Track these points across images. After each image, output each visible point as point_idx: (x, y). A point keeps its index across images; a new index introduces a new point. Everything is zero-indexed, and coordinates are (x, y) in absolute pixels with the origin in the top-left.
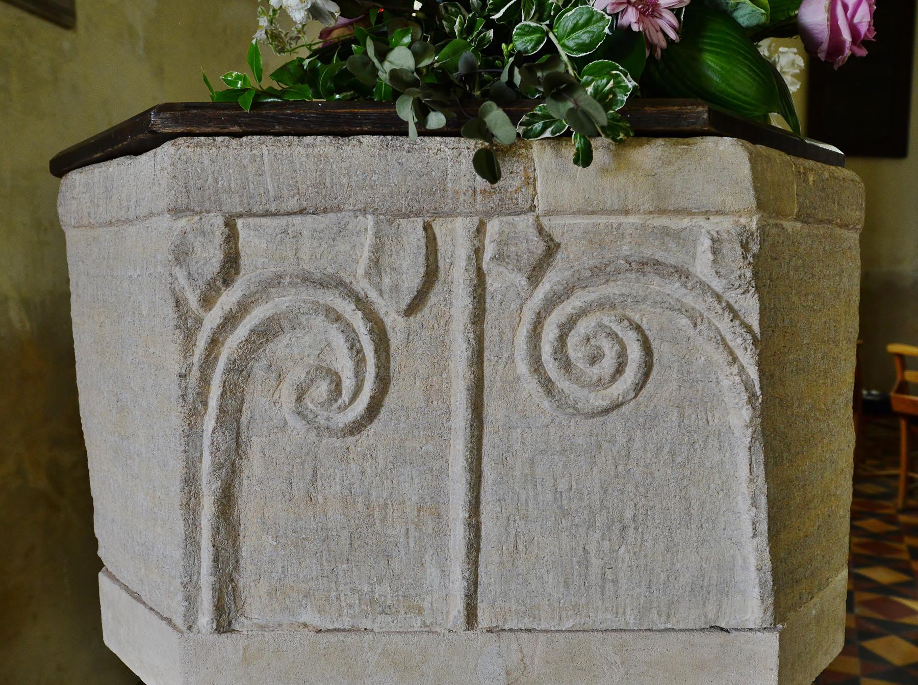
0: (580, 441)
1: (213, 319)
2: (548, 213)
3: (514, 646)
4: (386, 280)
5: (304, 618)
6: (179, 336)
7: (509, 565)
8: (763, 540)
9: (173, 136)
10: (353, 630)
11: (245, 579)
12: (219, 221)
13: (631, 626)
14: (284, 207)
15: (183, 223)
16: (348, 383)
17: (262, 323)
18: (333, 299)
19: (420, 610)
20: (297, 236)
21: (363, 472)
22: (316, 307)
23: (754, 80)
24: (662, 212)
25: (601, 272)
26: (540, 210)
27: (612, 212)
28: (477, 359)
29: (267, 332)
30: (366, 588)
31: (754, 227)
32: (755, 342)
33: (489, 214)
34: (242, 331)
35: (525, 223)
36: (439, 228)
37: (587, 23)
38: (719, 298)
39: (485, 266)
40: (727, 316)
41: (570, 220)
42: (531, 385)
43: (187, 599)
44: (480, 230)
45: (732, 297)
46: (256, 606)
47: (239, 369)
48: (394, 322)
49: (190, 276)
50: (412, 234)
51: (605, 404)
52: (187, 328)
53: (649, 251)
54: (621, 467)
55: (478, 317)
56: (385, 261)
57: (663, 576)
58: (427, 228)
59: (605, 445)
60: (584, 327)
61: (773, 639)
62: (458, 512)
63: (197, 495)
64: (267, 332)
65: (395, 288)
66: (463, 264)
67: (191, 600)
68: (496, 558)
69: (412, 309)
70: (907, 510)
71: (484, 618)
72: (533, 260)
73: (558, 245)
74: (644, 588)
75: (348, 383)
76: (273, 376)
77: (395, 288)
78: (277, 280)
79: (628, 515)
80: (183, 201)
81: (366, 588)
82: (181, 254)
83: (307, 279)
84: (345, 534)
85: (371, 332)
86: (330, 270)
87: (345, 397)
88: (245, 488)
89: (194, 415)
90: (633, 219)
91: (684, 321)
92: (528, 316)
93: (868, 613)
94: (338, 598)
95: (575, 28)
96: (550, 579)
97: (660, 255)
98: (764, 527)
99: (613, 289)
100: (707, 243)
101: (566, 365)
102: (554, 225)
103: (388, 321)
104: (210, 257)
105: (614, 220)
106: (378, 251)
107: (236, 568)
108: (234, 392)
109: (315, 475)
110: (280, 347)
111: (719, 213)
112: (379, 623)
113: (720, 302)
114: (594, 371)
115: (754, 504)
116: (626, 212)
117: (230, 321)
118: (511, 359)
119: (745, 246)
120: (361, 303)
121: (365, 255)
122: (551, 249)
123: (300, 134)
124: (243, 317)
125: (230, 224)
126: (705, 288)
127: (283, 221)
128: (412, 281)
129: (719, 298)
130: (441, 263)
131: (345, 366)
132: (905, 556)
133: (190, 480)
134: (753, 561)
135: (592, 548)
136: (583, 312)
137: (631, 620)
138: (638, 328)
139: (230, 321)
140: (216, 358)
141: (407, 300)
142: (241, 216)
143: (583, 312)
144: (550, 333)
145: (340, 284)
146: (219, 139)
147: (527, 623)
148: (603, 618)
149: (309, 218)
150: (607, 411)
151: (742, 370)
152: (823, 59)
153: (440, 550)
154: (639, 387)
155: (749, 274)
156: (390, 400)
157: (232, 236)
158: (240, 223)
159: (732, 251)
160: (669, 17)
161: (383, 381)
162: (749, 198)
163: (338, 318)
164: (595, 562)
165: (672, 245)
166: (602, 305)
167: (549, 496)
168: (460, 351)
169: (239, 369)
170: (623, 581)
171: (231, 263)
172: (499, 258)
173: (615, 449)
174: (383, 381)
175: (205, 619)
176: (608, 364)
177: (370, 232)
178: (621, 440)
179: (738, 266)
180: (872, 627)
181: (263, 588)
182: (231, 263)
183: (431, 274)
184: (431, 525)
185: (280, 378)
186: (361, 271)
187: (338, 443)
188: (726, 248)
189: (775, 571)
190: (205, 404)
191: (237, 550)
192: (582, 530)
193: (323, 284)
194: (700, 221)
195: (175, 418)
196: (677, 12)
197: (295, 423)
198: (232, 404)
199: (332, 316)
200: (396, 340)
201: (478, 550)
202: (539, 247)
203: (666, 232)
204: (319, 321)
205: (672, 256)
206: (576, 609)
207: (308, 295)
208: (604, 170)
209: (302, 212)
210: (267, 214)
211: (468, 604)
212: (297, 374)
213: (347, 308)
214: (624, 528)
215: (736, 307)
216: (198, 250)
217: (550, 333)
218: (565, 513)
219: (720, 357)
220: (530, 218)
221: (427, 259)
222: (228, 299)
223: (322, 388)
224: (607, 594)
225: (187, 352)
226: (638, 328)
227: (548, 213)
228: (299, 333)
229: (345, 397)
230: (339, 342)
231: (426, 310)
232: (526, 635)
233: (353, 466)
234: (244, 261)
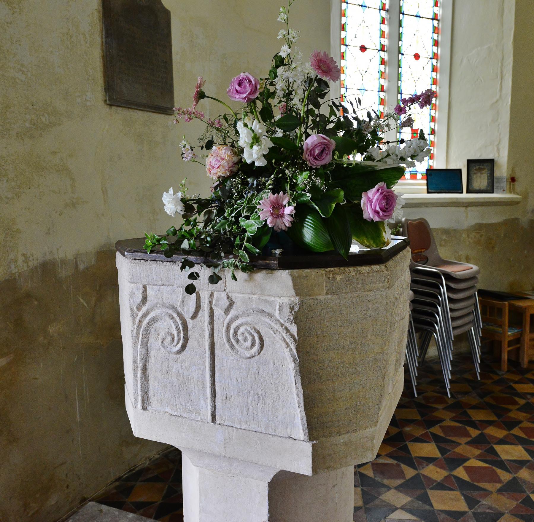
0: (243, 366)
1: (140, 314)
3: (227, 431)
7: (224, 403)
10: (180, 416)
11: (151, 393)
12: (142, 286)
13: (263, 432)
15: (132, 285)
17: (152, 318)
19: (200, 414)
20: (162, 292)
21: (182, 366)
26: (228, 291)
28: (212, 335)
29: (154, 320)
31: (297, 301)
38: (282, 325)
39: (213, 307)
40: (285, 332)
46: (154, 404)
47: (147, 331)
49: (133, 301)
51: (249, 355)
54: (256, 377)
56: (185, 302)
57: (272, 416)
59: (251, 369)
60: (242, 330)
63: (137, 366)
64: (154, 320)
65: (188, 311)
68: (220, 401)
73: (234, 302)
74: (266, 419)
76: (156, 333)
79: (260, 393)
81: (184, 404)
83: (164, 306)
84: (177, 385)
85: (182, 323)
86: (171, 303)
88: (150, 366)
92: (225, 324)
94: (176, 405)
96: (237, 411)
97: (264, 309)
98: (302, 405)
100: (278, 307)
101: (237, 341)
102: (233, 296)
107: (148, 390)
109: (168, 365)
110: (158, 325)
112: (188, 416)
113: (282, 327)
115: (298, 396)
117: (145, 316)
119: (292, 309)
120: (179, 314)
122: (231, 304)
124: (148, 315)
125: (145, 287)
128: (192, 309)
129: (282, 325)
130: (201, 304)
131: (175, 333)
135: (249, 402)
137: (263, 429)
139: (145, 316)
140: (141, 326)
144: (232, 331)
146: (142, 261)
147: (231, 424)
148: (254, 427)
149: (165, 287)
151: (291, 350)
153: (204, 395)
155: (292, 318)
156: (188, 345)
158: (147, 286)
159: (287, 310)
162: (293, 292)
164: (251, 408)
165: (268, 306)
167: (235, 383)
170: (260, 415)
171: (145, 299)
173: (254, 370)
174: (186, 339)
175: (139, 405)
176: (249, 343)
182: (145, 299)
184: (201, 387)
190: (139, 340)
191: (148, 385)
192: (246, 396)
198: (145, 341)
199: (171, 317)
201: (215, 397)
202: (227, 303)
205: (268, 309)
206: (246, 423)
211: (212, 414)
212: (162, 334)
214: (259, 397)
215: (289, 328)
216: (136, 294)
219: (284, 345)
220: (225, 293)
221: (196, 303)
222: (144, 309)
223: (169, 339)
224: (255, 419)
225: (134, 323)
231: (198, 318)
232: (230, 428)
233: (179, 364)
234: (148, 298)
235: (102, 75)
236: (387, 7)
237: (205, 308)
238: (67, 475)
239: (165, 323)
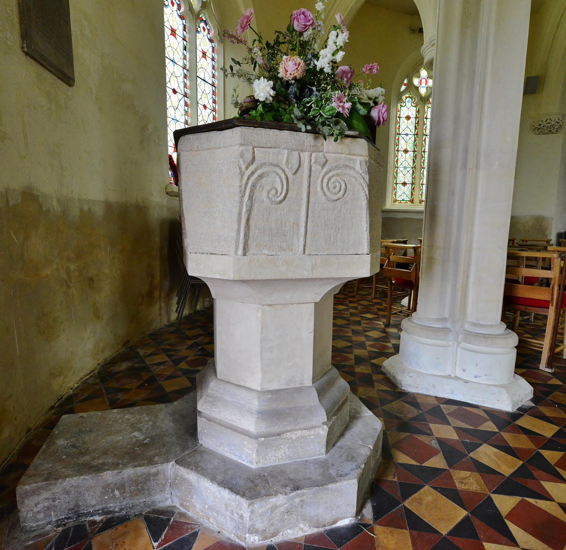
2: (326, 153)
4: (290, 166)
5: (264, 252)
6: (240, 177)
8: (368, 232)
9: (238, 126)
12: (251, 148)
14: (267, 146)
15: (242, 148)
16: (279, 191)
19: (292, 250)
22: (273, 172)
24: (350, 154)
25: (337, 167)
27: (340, 153)
28: (309, 187)
29: (261, 177)
30: (280, 244)
33: (313, 152)
35: (321, 154)
37: (332, 109)
41: (330, 155)
42: (321, 194)
43: (236, 246)
45: (363, 175)
46: (252, 249)
48: (290, 176)
50: (296, 154)
51: (337, 198)
52: (242, 174)
53: (347, 163)
55: (310, 176)
58: (299, 154)
60: (333, 180)
61: (369, 256)
62: (303, 224)
64: (261, 177)
65: (292, 168)
66: (307, 163)
69: (295, 173)
70: (374, 298)
72: (323, 163)
75: (279, 191)
77: (292, 168)
78: (264, 164)
79: (340, 226)
80: (243, 142)
82: (242, 156)
87: (279, 194)
90: (343, 155)
91: (354, 180)
92: (321, 177)
93: (366, 326)
95: (329, 111)
97: (349, 164)
99: (339, 171)
100: (359, 162)
101: (329, 188)
102: (328, 155)
103: (289, 176)
104: (249, 157)
105: (339, 155)
106: (288, 158)
108: (252, 191)
110: (264, 181)
111: (361, 156)
114: (335, 190)
115: (367, 223)
116: (342, 154)
117: (253, 173)
118: (316, 187)
120: (284, 171)
122: (327, 161)
123: (271, 129)
127: (266, 149)
128: (296, 167)
132: (376, 311)
133: (240, 214)
134: (366, 237)
135: (332, 234)
136: (333, 176)
139: (253, 173)
141: (294, 171)
142: (256, 147)
143: (333, 176)
144: (325, 181)
149: (272, 149)
150: (337, 200)
154: (344, 195)
156: (288, 196)
158: (255, 149)
159: (364, 164)
160: (347, 110)
161: (287, 191)
164: (332, 238)
166: (338, 175)
168: (305, 184)
171: (254, 158)
172: (315, 162)
175: (240, 252)
176: (338, 189)
177: (286, 154)
178: (339, 207)
180: (368, 329)
181: (254, 244)
182: (254, 158)
185: (263, 189)
186: (284, 163)
187: (275, 206)
188: (363, 163)
189: (371, 239)
194: (357, 157)
195: (237, 198)
196: (348, 109)
197: (266, 200)
202: (324, 160)
203: (350, 159)
204: (274, 175)
205: (352, 165)
208: (338, 144)
209: (271, 148)
210: (263, 147)
213: (280, 172)
217: (325, 181)
219: (361, 188)
220: (322, 153)
222: (252, 168)
223: (273, 192)
227: (326, 153)
228: (268, 178)
229: (279, 194)
230: (278, 180)
234: (256, 159)
235: (18, 21)
236: (187, 68)
237: (305, 165)
238: (14, 408)
239: (270, 179)
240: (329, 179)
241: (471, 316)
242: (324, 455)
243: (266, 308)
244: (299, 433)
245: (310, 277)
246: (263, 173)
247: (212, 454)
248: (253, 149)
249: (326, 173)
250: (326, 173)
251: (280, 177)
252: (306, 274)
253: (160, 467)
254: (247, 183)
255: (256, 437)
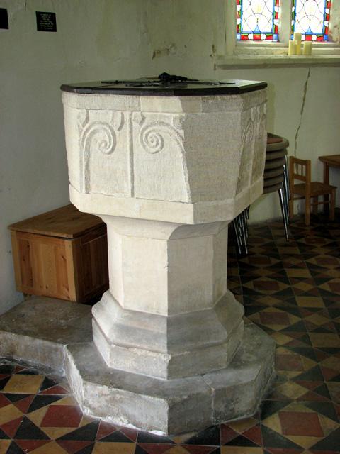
1: (84, 129)
15: (79, 111)
16: (108, 144)
18: (105, 126)
23: (195, 82)
25: (152, 124)
28: (131, 140)
29: (94, 132)
32: (183, 140)
34: (89, 133)
36: (124, 113)
44: (131, 114)
46: (93, 190)
47: (89, 140)
48: (117, 132)
50: (119, 114)
58: (122, 113)
60: (150, 135)
64: (94, 132)
67: (81, 187)
71: (135, 196)
75: (108, 144)
82: (79, 117)
89: (81, 148)
91: (168, 135)
99: (155, 128)
102: (144, 114)
104: (83, 117)
110: (97, 136)
115: (185, 175)
117: (87, 130)
120: (110, 127)
121: (111, 118)
122: (144, 118)
126: (172, 128)
128: (119, 124)
131: (108, 140)
133: (81, 161)
138: (160, 136)
139: (87, 130)
145: (107, 124)
152: (89, 123)
153: (127, 180)
154: (161, 148)
156: (116, 148)
157: (88, 114)
158: (89, 111)
163: (106, 131)
169: (89, 140)
171: (87, 119)
174: (115, 144)
175: (84, 190)
176: (155, 143)
179: (178, 124)
182: (87, 119)
183: (122, 123)
187: (107, 156)
193: (103, 124)
198: (88, 147)
200: (117, 135)
202: (141, 118)
203: (165, 116)
207: (101, 126)
212: (99, 141)
213: (108, 128)
218: (150, 174)
222: (87, 125)
223: (103, 145)
225: (80, 134)
226: (160, 136)
237: (127, 123)
240: (147, 135)
241: (68, 248)
242: (166, 380)
243: (127, 239)
244: (144, 352)
245: (139, 217)
246: (95, 130)
247: (95, 348)
248: (88, 112)
249: (144, 129)
250: (144, 129)
251: (108, 133)
252: (135, 215)
253: (60, 346)
254: (84, 138)
255: (110, 344)
